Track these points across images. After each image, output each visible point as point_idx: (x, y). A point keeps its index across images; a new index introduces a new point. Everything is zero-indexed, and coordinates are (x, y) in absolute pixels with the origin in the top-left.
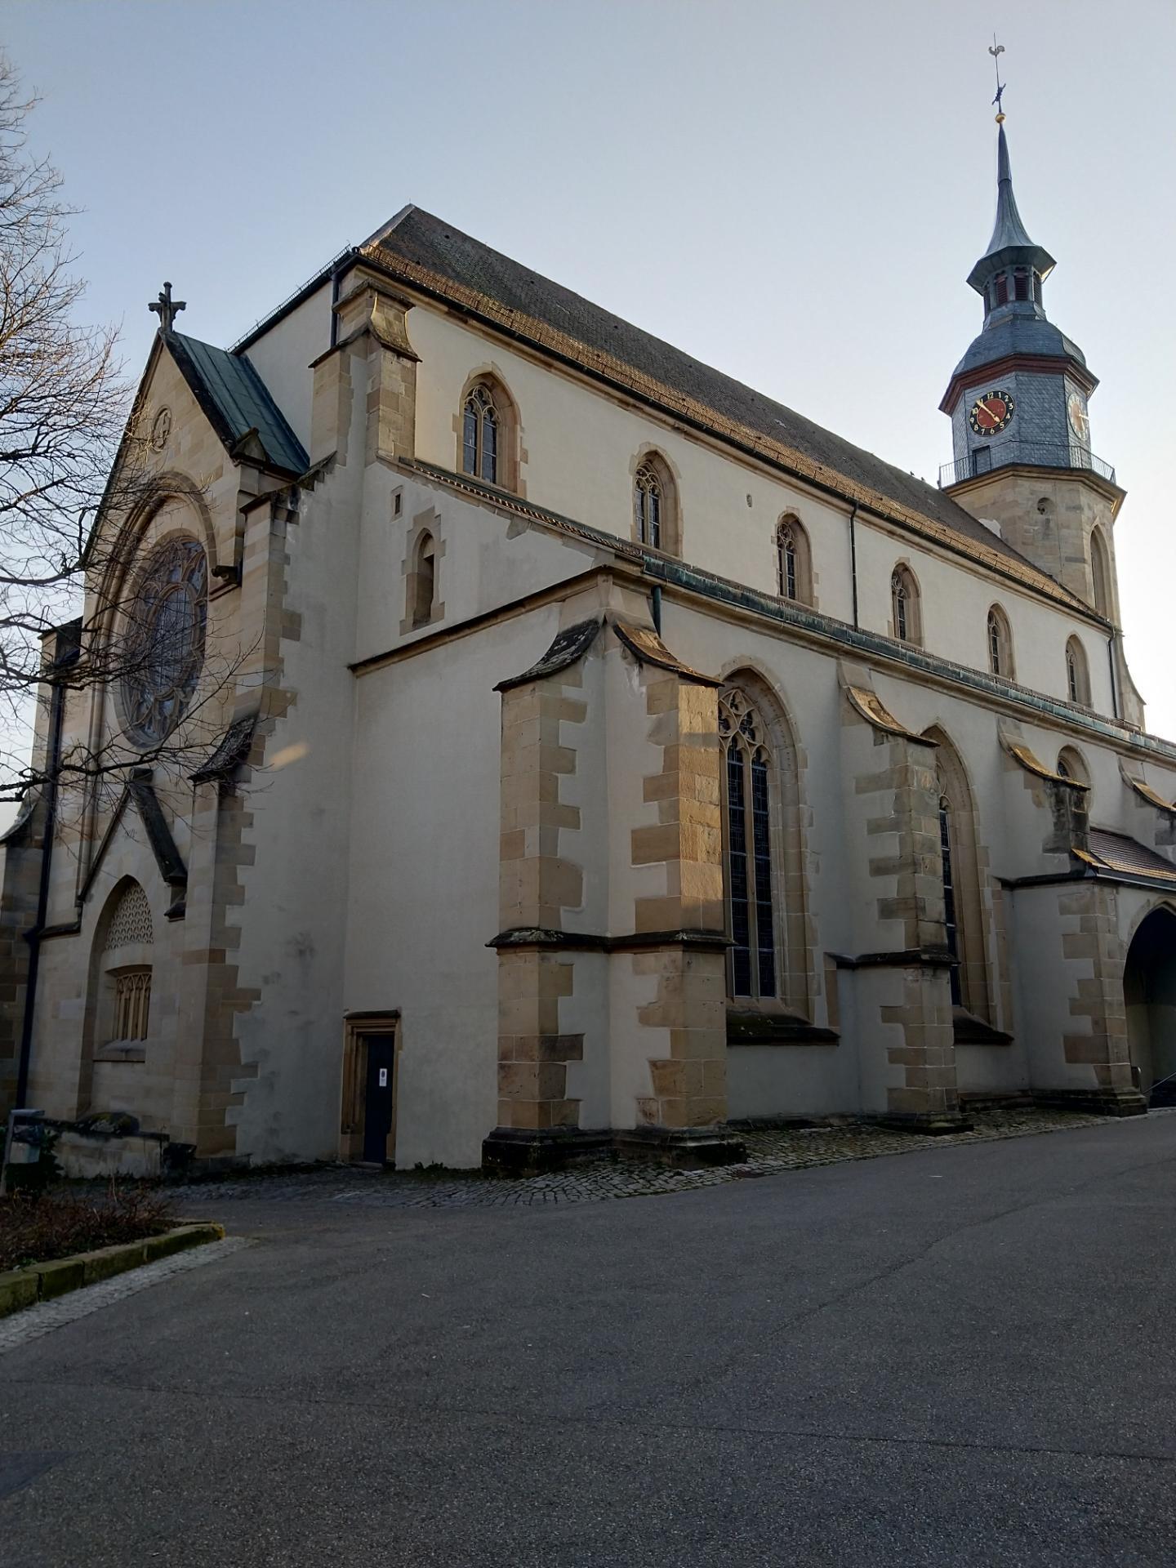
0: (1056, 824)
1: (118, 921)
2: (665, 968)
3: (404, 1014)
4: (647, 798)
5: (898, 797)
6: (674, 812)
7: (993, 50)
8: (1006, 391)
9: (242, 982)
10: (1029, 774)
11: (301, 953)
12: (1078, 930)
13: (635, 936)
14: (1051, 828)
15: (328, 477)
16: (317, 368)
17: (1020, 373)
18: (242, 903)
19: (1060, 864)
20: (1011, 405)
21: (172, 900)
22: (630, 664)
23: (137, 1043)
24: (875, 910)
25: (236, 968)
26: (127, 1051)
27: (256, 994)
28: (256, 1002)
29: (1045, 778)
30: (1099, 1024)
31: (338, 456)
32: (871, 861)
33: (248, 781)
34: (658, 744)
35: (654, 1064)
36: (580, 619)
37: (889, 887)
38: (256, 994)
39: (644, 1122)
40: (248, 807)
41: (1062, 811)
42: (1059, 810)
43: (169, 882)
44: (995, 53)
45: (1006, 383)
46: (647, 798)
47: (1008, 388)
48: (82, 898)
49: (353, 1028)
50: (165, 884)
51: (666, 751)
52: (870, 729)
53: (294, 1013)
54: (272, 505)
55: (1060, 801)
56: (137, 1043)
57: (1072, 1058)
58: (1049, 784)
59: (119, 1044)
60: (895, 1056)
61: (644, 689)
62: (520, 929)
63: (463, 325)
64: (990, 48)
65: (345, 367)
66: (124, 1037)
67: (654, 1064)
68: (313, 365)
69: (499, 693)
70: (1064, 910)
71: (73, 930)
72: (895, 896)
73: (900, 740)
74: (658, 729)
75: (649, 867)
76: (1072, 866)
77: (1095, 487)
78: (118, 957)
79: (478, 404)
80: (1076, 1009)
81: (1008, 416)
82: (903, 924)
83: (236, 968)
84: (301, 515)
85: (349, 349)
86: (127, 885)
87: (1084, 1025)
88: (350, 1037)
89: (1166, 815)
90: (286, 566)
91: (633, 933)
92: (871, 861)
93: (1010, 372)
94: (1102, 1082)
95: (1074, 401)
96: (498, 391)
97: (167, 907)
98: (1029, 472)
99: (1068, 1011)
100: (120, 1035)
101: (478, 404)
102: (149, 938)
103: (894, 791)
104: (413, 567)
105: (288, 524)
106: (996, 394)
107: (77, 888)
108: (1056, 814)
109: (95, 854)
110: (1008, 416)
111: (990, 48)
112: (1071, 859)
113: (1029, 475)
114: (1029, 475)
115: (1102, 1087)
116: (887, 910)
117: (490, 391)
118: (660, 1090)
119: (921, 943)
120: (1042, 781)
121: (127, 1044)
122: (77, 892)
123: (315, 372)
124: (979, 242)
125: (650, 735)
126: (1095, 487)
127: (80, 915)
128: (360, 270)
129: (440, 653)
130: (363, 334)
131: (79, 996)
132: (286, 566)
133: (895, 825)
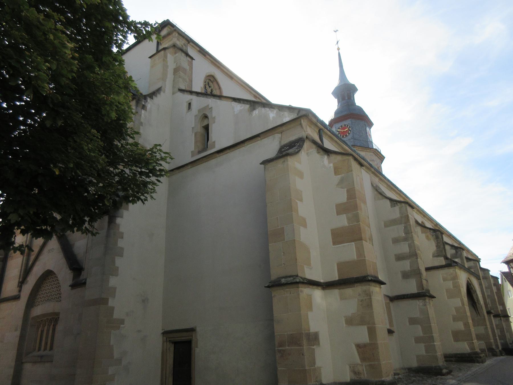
0: (437, 246)
1: (38, 297)
2: (359, 295)
3: (198, 329)
4: (338, 213)
5: (405, 227)
6: (357, 218)
7: (335, 31)
8: (348, 124)
9: (116, 316)
10: (422, 228)
11: (143, 301)
12: (452, 287)
13: (338, 280)
14: (435, 248)
15: (158, 95)
16: (152, 58)
17: (352, 119)
18: (117, 275)
19: (441, 261)
20: (350, 128)
21: (73, 280)
22: (322, 155)
23: (47, 352)
24: (400, 275)
25: (113, 308)
26: (42, 357)
27: (122, 322)
28: (122, 326)
29: (430, 229)
30: (466, 324)
31: (162, 88)
32: (395, 255)
33: (122, 217)
34: (342, 188)
35: (358, 346)
36: (293, 138)
37: (406, 265)
38: (122, 322)
39: (355, 377)
40: (122, 229)
41: (438, 241)
42: (437, 241)
43: (72, 270)
44: (336, 32)
45: (348, 122)
46: (338, 213)
47: (349, 124)
48: (22, 283)
49: (167, 338)
50: (70, 271)
51: (348, 191)
52: (388, 202)
53: (139, 331)
54: (136, 101)
55: (437, 238)
56: (47, 352)
57: (456, 339)
58: (432, 231)
59: (36, 353)
60: (418, 340)
61: (331, 165)
62: (286, 277)
63: (204, 57)
64: (334, 31)
65: (166, 57)
66: (45, 349)
67: (358, 346)
68: (150, 57)
69: (263, 166)
70: (445, 280)
71: (16, 298)
72: (409, 269)
73: (403, 204)
74: (341, 181)
75: (344, 246)
76: (445, 262)
77: (377, 155)
78: (38, 311)
79: (207, 87)
80: (455, 319)
81: (349, 132)
82: (415, 281)
83: (113, 308)
84: (148, 108)
85: (167, 51)
86: (48, 274)
87: (460, 326)
88: (165, 343)
89: (454, 248)
90: (141, 127)
91: (337, 279)
92: (395, 255)
93: (349, 119)
94: (471, 349)
95: (368, 129)
96: (215, 83)
97: (70, 282)
98: (358, 148)
99: (452, 320)
100: (37, 348)
101: (207, 87)
102: (58, 299)
103: (403, 225)
104: (200, 129)
105: (143, 110)
106: (345, 125)
107: (19, 278)
108: (436, 242)
109: (30, 263)
110: (349, 132)
111: (334, 31)
112: (444, 259)
113: (358, 149)
114: (358, 149)
115: (471, 351)
116: (406, 275)
117: (212, 83)
118: (363, 359)
119: (424, 289)
120: (428, 230)
121: (41, 353)
122: (19, 280)
123: (151, 60)
124: (335, 82)
125: (338, 185)
126: (377, 155)
127: (20, 291)
128: (169, 27)
129: (213, 162)
130: (172, 47)
131: (16, 330)
132: (141, 127)
133: (405, 239)
